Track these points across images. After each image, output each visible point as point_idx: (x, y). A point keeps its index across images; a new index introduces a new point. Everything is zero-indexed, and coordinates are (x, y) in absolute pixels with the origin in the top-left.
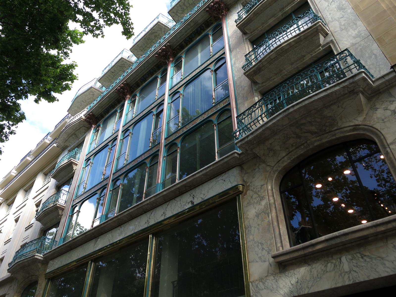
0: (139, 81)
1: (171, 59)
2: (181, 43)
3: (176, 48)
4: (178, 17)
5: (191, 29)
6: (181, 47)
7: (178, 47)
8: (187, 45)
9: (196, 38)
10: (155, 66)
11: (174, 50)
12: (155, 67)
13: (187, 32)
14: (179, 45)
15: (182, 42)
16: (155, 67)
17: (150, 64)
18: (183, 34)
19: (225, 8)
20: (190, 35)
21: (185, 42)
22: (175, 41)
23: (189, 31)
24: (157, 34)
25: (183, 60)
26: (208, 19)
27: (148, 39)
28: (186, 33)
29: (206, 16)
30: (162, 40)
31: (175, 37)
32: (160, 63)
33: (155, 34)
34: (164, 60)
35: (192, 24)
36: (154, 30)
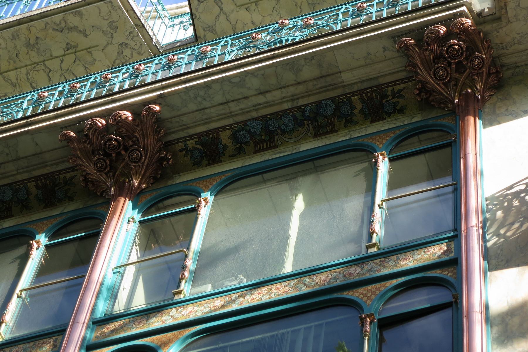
0: (229, 133)
1: (136, 183)
2: (216, 130)
3: (181, 145)
4: (217, 10)
5: (292, 90)
6: (209, 150)
7: (191, 143)
8: (239, 152)
9: (298, 142)
10: (36, 178)
11: (167, 145)
12: (31, 186)
13: (269, 97)
14: (199, 135)
15: (224, 128)
16: (31, 186)
17: (18, 159)
18: (246, 98)
19: (489, 74)
20: (276, 113)
21: (234, 137)
22: (192, 107)
23: (277, 95)
24: (84, 42)
25: (204, 212)
26: (388, 84)
27: (28, 45)
28: (261, 99)
29: (388, 67)
30: (119, 80)
31: (202, 93)
32: (68, 176)
33: (74, 37)
34: (99, 170)
35: (307, 73)
36: (78, 18)
